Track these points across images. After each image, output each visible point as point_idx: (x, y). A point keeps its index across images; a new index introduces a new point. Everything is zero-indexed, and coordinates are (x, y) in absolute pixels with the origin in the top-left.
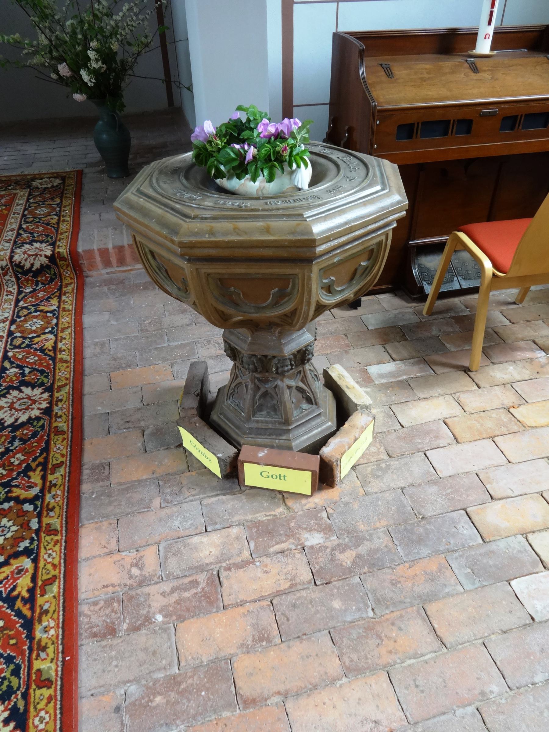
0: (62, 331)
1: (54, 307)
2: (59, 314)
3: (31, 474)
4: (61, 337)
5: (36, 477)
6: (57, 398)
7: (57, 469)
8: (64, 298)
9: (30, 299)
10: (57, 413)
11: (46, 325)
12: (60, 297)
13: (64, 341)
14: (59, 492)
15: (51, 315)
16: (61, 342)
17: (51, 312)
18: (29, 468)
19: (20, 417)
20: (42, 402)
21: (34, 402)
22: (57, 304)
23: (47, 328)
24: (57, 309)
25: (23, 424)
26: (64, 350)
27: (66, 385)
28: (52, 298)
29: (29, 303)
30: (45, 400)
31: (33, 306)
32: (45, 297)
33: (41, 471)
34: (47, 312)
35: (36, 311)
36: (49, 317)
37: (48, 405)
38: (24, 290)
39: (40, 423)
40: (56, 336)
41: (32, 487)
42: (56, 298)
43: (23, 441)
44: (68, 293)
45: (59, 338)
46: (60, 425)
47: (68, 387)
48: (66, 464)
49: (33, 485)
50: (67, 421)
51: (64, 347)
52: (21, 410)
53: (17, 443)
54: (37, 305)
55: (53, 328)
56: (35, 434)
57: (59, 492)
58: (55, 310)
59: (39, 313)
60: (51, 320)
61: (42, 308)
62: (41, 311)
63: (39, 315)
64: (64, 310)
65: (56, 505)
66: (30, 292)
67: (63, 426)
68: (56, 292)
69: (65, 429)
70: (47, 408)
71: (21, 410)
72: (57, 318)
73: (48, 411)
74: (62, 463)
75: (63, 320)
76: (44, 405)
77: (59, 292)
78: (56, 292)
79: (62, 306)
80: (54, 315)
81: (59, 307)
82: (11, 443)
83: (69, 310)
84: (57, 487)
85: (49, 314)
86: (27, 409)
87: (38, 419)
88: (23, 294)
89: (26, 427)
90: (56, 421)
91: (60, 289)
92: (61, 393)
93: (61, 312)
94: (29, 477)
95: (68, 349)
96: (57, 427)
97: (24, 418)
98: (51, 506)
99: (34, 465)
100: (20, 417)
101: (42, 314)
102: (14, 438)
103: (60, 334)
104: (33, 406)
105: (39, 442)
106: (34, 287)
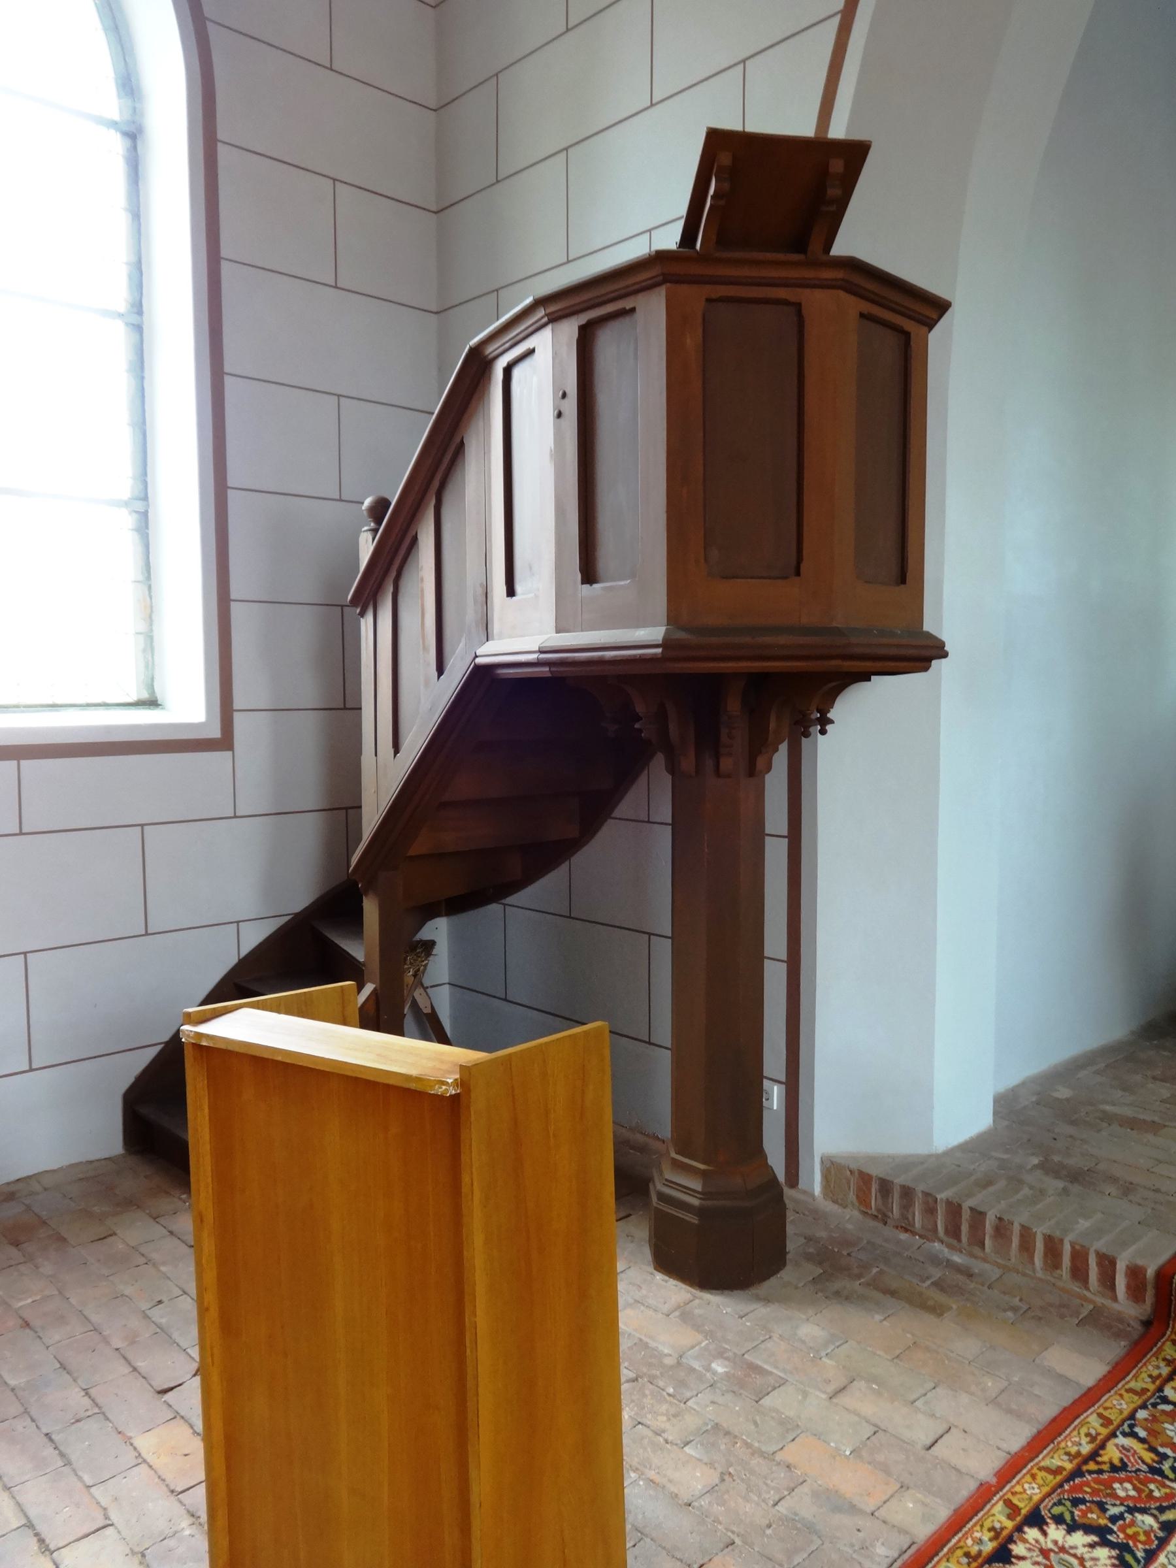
0: (1145, 1391)
1: (1121, 1440)
2: (1122, 1424)
3: (1116, 1462)
4: (1153, 1382)
5: (1112, 1453)
6: (1071, 1461)
7: (1054, 1468)
8: (1086, 1449)
9: (1157, 1494)
10: (991, 1540)
11: (1163, 1418)
12: (1094, 1456)
13: (1155, 1373)
14: (969, 1542)
15: (1137, 1430)
16: (1160, 1375)
17: (1134, 1435)
18: (1114, 1468)
19: (1084, 1546)
20: (1033, 1542)
21: (1045, 1553)
22: (1110, 1446)
23: (1163, 1411)
24: (1118, 1433)
25: (1088, 1529)
26: (1164, 1359)
27: (1129, 1391)
28: (1112, 1464)
29: (1165, 1486)
30: (1025, 1541)
31: (1160, 1472)
32: (1123, 1475)
33: (1100, 1456)
34: (1142, 1441)
35: (1164, 1457)
36: (1145, 1429)
37: (1026, 1529)
38: (1156, 1526)
39: (1057, 1510)
40: (1160, 1389)
41: (1123, 1446)
42: (1099, 1459)
43: (1102, 1507)
44: (1067, 1454)
45: (1158, 1382)
46: (1003, 1519)
47: (1042, 1464)
48: (1123, 1386)
49: (1121, 1448)
50: (1161, 1349)
51: (1162, 1364)
52: (1075, 1556)
53: (1114, 1511)
54: (1153, 1470)
55: (1154, 1405)
56: (1076, 1502)
57: (969, 1542)
58: (1125, 1435)
59: (1161, 1450)
60: (1146, 1420)
61: (1148, 1456)
62: (1152, 1449)
63: (1162, 1446)
64: (1107, 1422)
65: (985, 1531)
66: (1144, 1511)
67: (1000, 1513)
68: (1090, 1472)
69: (1000, 1506)
70: (1031, 1525)
71: (1075, 1556)
72: (1132, 1416)
73: (1035, 1519)
74: (1040, 1469)
75: (1125, 1406)
76: (1032, 1533)
77: (1085, 1468)
78: (1090, 1472)
79: (1105, 1432)
80: (1131, 1426)
81: (1113, 1435)
82: (1121, 1517)
83: (1100, 1416)
84: (965, 1549)
85: (1142, 1434)
86: (1063, 1549)
87: (1059, 1520)
88: (1164, 1517)
89: (1084, 1521)
90: (1002, 1529)
91: (1077, 1473)
92: (1060, 1463)
93: (1115, 1423)
94: (1121, 1460)
95: (1157, 1358)
96: (1102, 1425)
97: (1079, 1539)
98: (992, 1534)
99: (1106, 1467)
100: (1084, 1546)
101: (1154, 1443)
102: (1114, 1519)
103: (1152, 1387)
104: (1050, 1545)
105: (1079, 1488)
106: (1128, 1516)
